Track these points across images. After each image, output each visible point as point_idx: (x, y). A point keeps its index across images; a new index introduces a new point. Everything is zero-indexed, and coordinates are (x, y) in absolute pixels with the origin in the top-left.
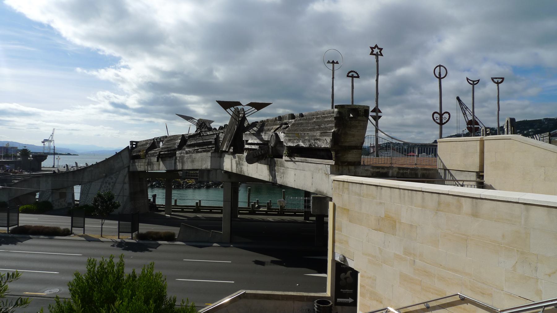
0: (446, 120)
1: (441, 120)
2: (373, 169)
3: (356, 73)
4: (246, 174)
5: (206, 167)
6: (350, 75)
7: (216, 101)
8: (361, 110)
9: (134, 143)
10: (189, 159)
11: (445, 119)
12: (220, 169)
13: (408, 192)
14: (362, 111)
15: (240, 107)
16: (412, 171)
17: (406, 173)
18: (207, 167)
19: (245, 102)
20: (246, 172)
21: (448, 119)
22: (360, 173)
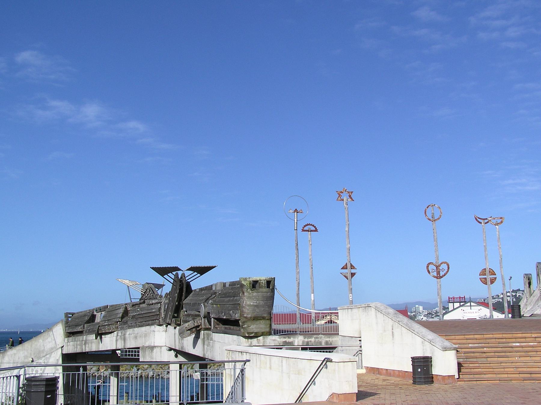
0: (445, 272)
1: (438, 273)
2: (280, 339)
3: (313, 226)
4: (187, 351)
5: (150, 344)
6: (306, 228)
7: (151, 267)
8: (262, 282)
9: (69, 315)
10: (131, 334)
11: (443, 271)
12: (166, 346)
13: (208, 357)
14: (263, 283)
15: (180, 273)
16: (316, 339)
17: (310, 341)
18: (151, 344)
19: (184, 266)
20: (186, 348)
21: (447, 270)
22: (268, 343)
